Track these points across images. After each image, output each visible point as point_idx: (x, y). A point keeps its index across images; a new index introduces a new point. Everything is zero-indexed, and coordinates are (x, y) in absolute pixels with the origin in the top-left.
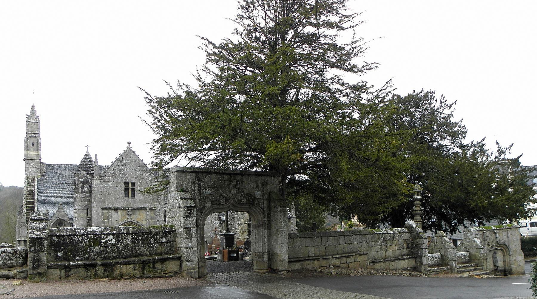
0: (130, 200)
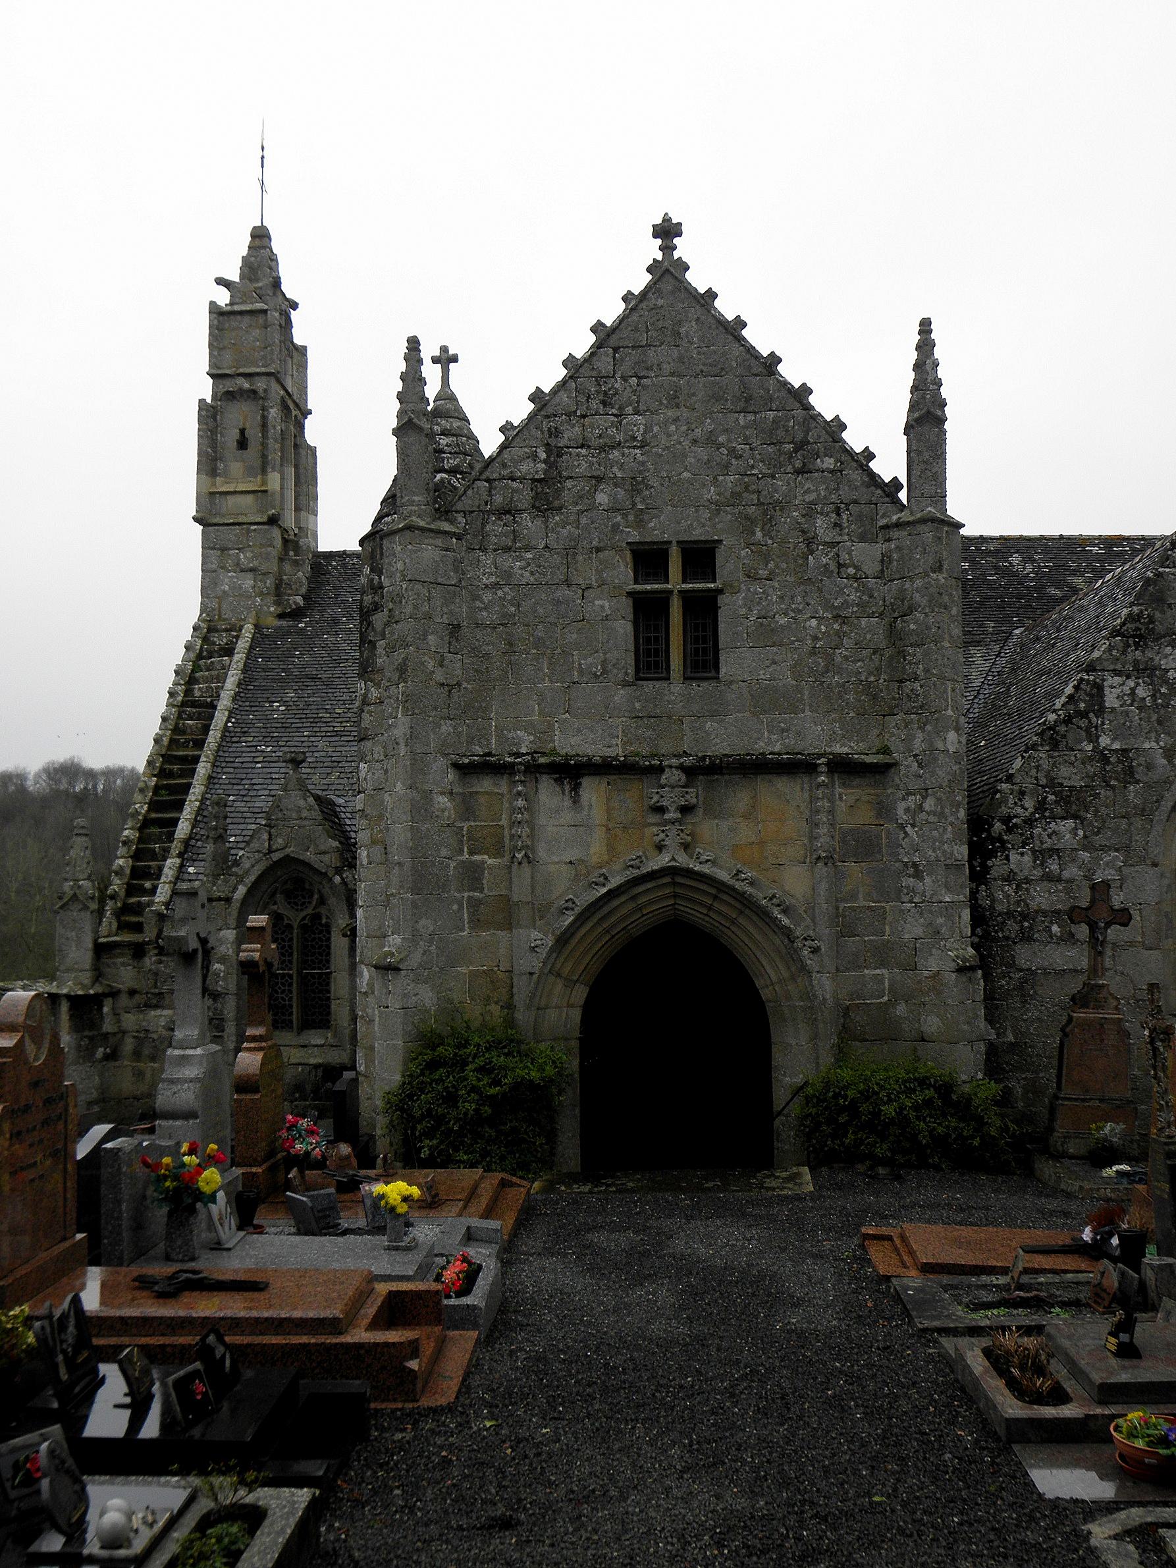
0: (675, 692)
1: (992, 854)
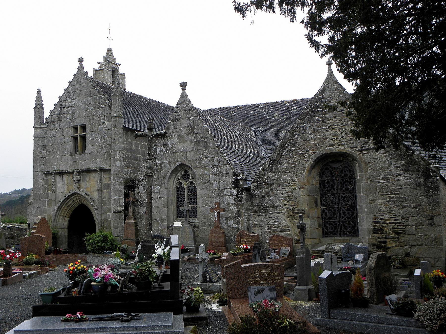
1: (136, 188)
